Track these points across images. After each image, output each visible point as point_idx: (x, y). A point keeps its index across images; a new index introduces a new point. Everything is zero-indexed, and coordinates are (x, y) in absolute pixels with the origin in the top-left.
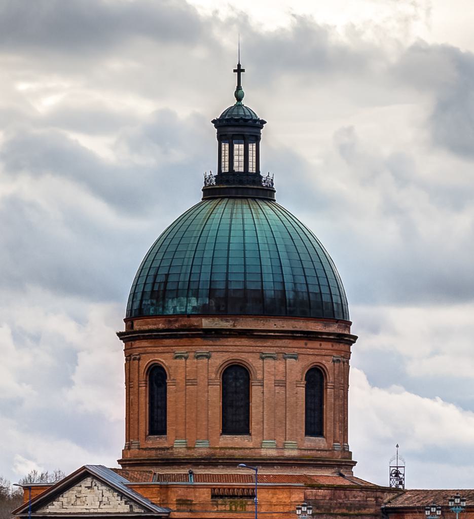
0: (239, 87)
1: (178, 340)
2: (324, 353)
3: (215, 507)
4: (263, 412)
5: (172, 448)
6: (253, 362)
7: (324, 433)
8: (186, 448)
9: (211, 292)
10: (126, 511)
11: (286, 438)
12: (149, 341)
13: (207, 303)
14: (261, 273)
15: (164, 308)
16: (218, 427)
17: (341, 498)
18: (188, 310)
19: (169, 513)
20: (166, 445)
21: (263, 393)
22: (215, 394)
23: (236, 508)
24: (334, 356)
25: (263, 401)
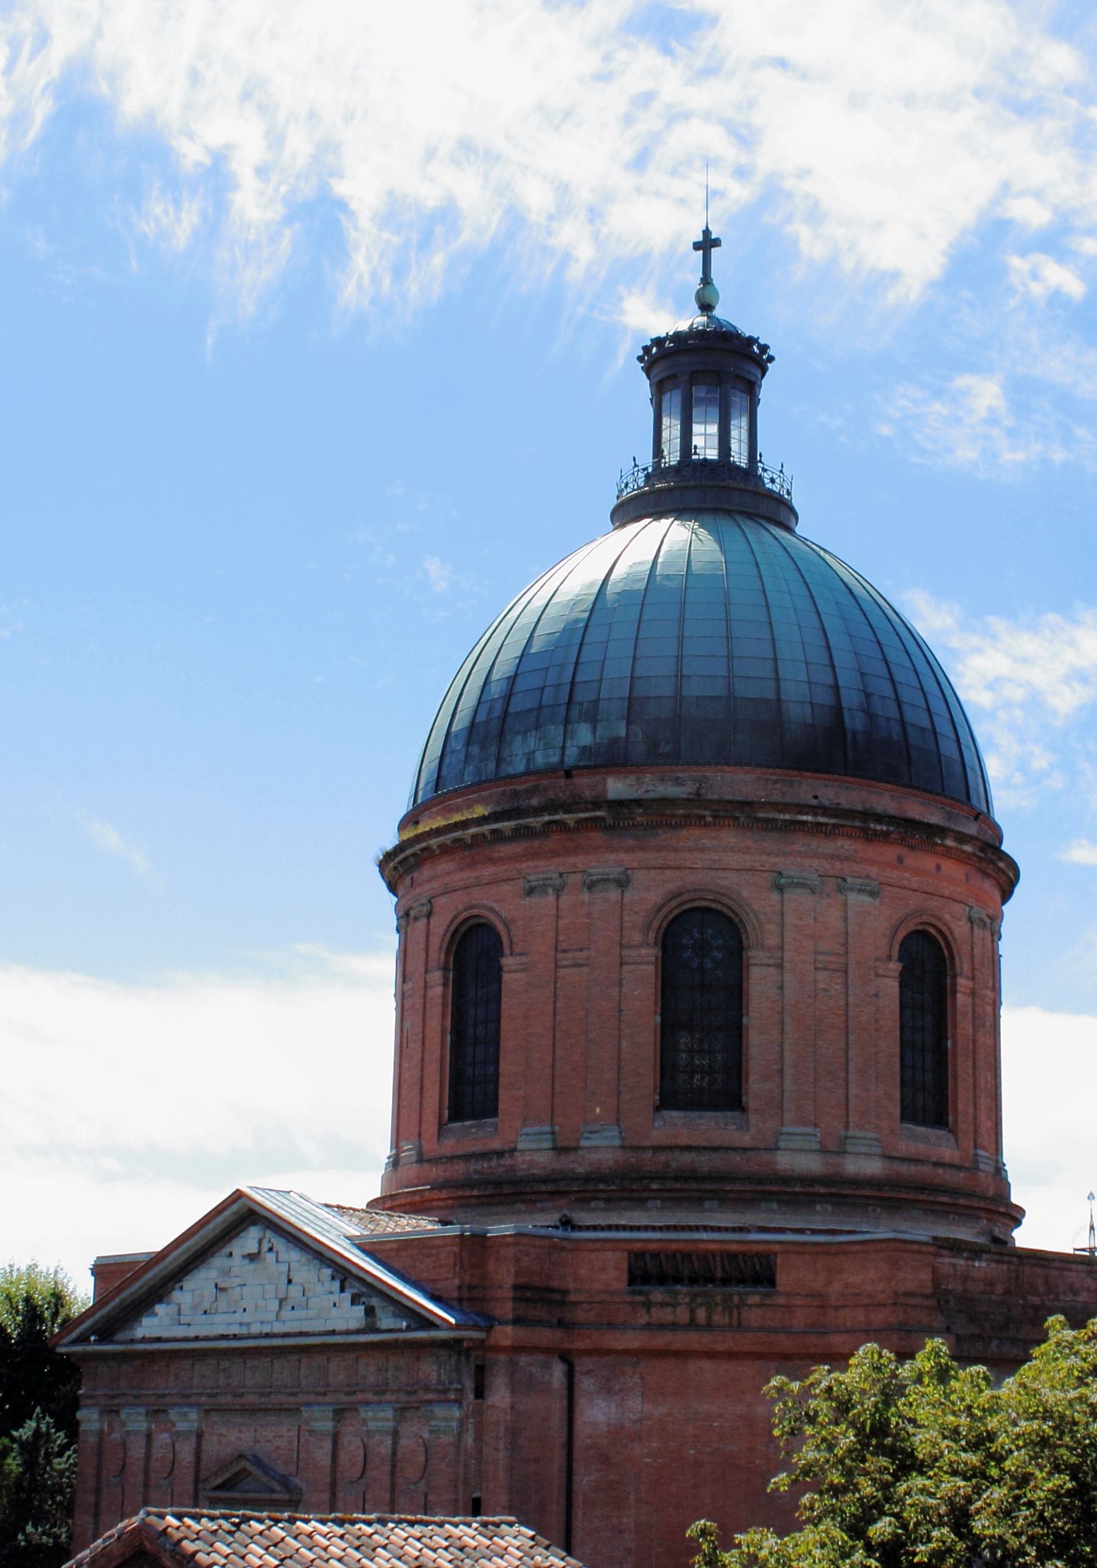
0: (706, 280)
3: (643, 1311)
4: (782, 1045)
5: (513, 1150)
6: (756, 901)
7: (950, 1118)
8: (553, 1149)
9: (633, 707)
10: (353, 1325)
11: (847, 1122)
13: (623, 734)
14: (775, 660)
15: (499, 759)
16: (645, 1081)
17: (1035, 1293)
18: (566, 759)
20: (496, 1145)
21: (781, 988)
23: (709, 1317)
25: (782, 1013)
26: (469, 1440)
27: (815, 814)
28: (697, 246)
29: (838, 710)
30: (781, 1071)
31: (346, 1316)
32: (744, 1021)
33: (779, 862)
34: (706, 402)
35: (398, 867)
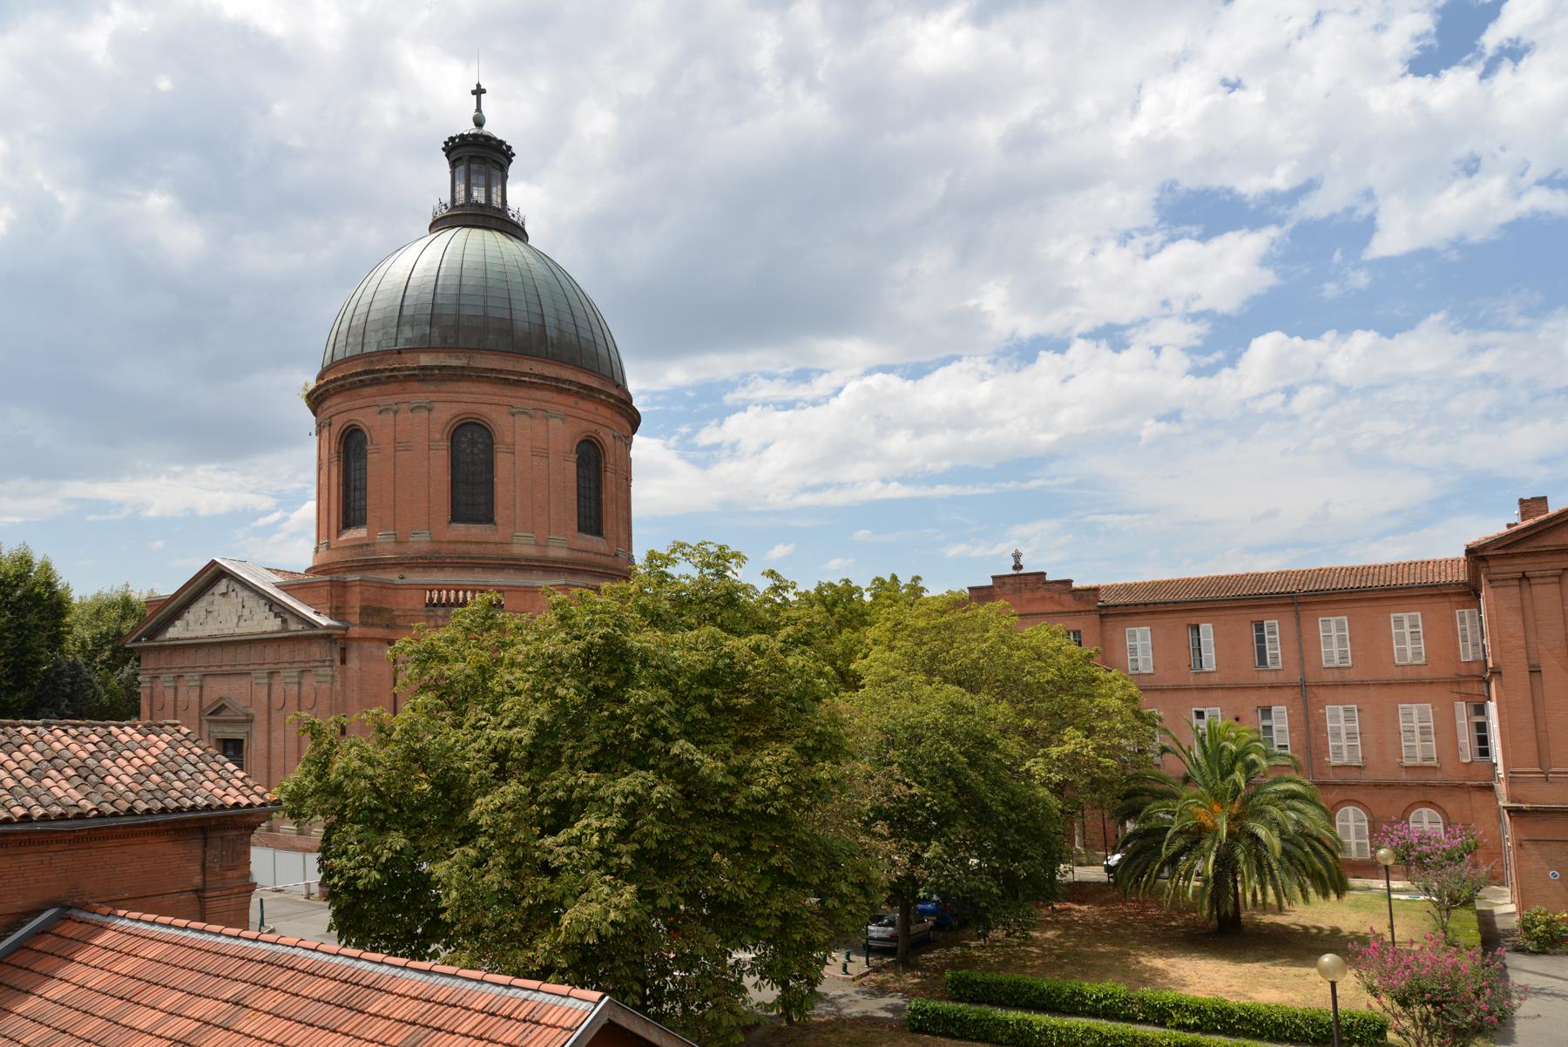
0: (479, 109)
6: (499, 419)
12: (1171, 996)
19: (347, 629)
22: (440, 462)
26: (338, 686)
28: (474, 93)
31: (272, 624)
33: (513, 401)
34: (479, 172)
35: (315, 400)
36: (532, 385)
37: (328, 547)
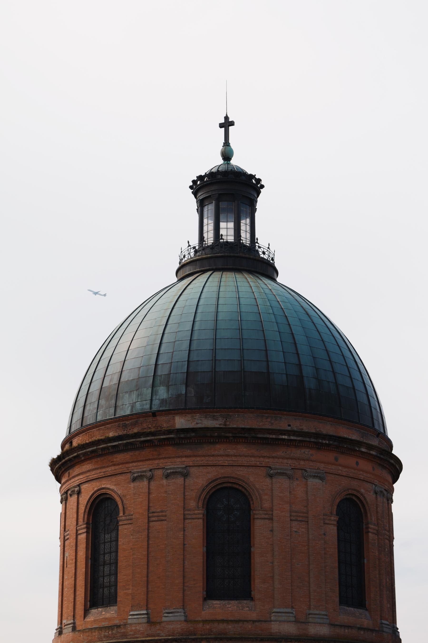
0: (227, 143)
1: (137, 453)
2: (362, 477)
4: (272, 563)
6: (256, 481)
12: (93, 460)
13: (184, 392)
14: (266, 350)
21: (272, 531)
24: (376, 485)
27: (289, 435)
28: (221, 126)
29: (301, 377)
30: (272, 577)
32: (252, 549)
35: (60, 467)
36: (289, 444)
37: (74, 629)
